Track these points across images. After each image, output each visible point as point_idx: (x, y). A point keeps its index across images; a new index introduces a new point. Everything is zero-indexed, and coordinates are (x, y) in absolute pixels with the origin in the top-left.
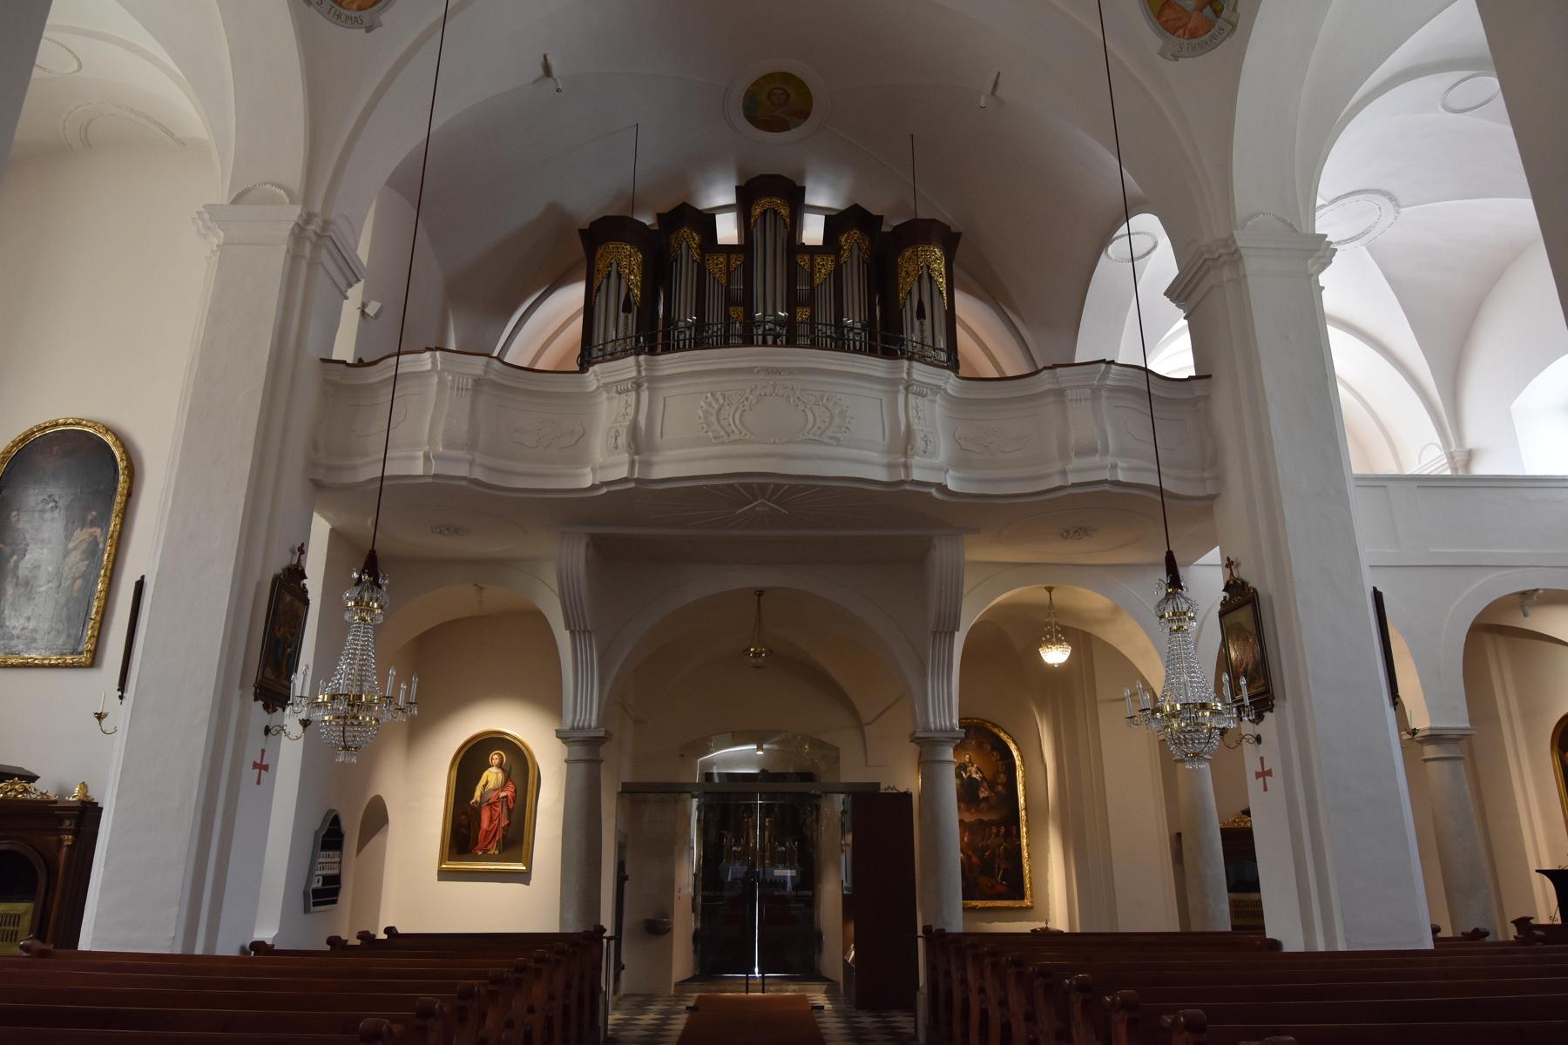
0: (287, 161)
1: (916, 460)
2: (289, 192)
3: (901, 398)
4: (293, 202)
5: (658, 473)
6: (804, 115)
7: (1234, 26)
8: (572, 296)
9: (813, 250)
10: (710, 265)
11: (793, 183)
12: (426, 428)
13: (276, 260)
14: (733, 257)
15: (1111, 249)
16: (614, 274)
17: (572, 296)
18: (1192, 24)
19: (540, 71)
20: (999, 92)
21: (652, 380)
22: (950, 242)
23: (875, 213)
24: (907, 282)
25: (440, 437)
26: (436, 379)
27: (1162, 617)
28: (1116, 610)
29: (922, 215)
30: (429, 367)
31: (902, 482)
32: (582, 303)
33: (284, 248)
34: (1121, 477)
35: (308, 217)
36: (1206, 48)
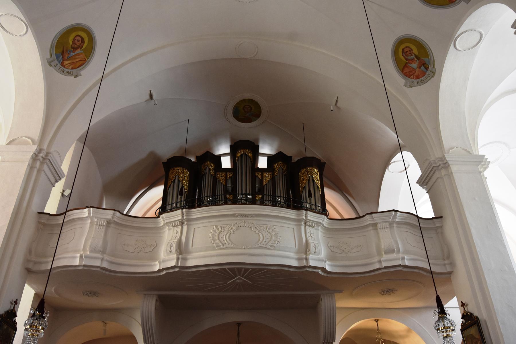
0: (35, 130)
1: (311, 256)
2: (33, 141)
3: (303, 228)
4: (34, 144)
5: (191, 263)
6: (258, 116)
7: (434, 73)
8: (158, 192)
9: (263, 170)
10: (218, 177)
11: (254, 143)
12: (82, 245)
13: (23, 169)
14: (228, 173)
15: (391, 167)
16: (176, 181)
17: (158, 192)
18: (416, 74)
19: (148, 97)
20: (338, 105)
21: (189, 220)
22: (321, 166)
23: (289, 155)
24: (303, 183)
25: (88, 247)
26: (89, 221)
27: (438, 330)
28: (409, 331)
29: (309, 155)
30: (87, 215)
31: (305, 267)
32: (161, 195)
33: (27, 163)
34: (407, 263)
35: (40, 151)
36: (423, 82)
